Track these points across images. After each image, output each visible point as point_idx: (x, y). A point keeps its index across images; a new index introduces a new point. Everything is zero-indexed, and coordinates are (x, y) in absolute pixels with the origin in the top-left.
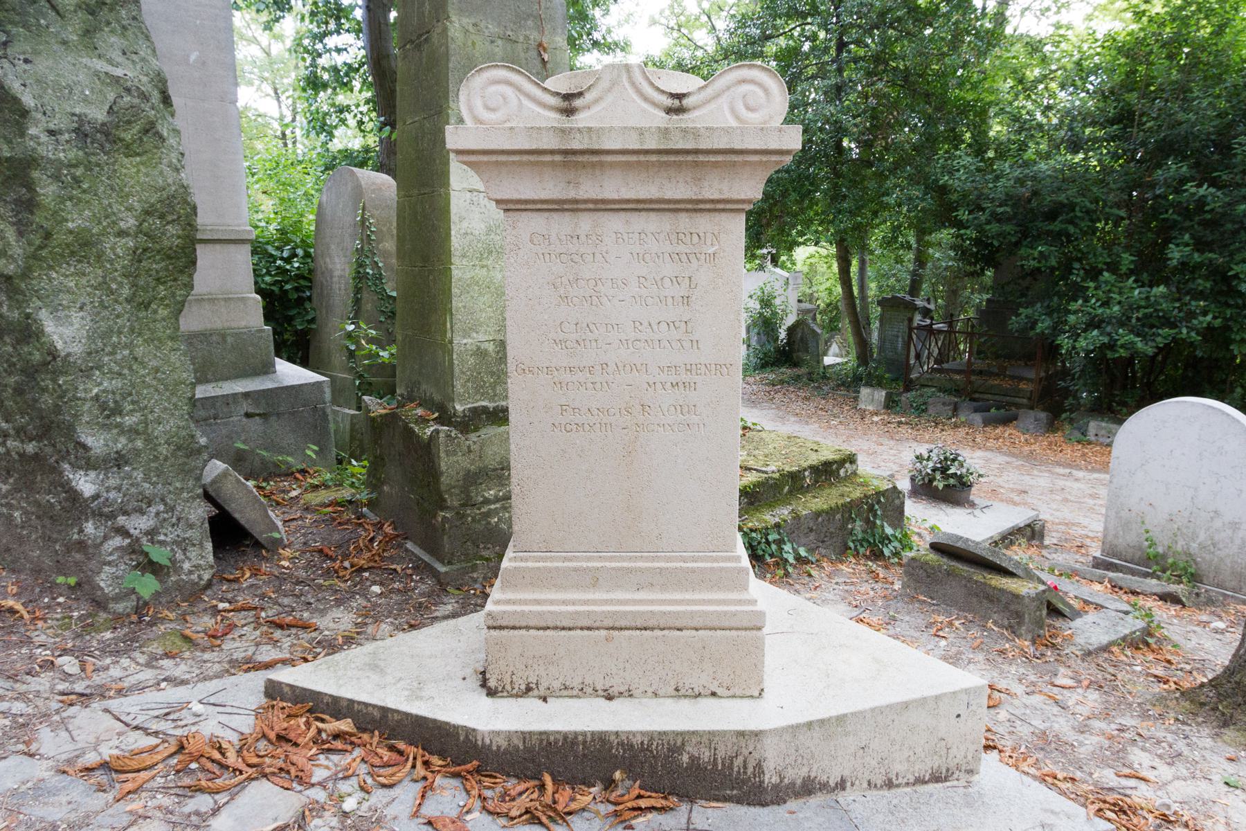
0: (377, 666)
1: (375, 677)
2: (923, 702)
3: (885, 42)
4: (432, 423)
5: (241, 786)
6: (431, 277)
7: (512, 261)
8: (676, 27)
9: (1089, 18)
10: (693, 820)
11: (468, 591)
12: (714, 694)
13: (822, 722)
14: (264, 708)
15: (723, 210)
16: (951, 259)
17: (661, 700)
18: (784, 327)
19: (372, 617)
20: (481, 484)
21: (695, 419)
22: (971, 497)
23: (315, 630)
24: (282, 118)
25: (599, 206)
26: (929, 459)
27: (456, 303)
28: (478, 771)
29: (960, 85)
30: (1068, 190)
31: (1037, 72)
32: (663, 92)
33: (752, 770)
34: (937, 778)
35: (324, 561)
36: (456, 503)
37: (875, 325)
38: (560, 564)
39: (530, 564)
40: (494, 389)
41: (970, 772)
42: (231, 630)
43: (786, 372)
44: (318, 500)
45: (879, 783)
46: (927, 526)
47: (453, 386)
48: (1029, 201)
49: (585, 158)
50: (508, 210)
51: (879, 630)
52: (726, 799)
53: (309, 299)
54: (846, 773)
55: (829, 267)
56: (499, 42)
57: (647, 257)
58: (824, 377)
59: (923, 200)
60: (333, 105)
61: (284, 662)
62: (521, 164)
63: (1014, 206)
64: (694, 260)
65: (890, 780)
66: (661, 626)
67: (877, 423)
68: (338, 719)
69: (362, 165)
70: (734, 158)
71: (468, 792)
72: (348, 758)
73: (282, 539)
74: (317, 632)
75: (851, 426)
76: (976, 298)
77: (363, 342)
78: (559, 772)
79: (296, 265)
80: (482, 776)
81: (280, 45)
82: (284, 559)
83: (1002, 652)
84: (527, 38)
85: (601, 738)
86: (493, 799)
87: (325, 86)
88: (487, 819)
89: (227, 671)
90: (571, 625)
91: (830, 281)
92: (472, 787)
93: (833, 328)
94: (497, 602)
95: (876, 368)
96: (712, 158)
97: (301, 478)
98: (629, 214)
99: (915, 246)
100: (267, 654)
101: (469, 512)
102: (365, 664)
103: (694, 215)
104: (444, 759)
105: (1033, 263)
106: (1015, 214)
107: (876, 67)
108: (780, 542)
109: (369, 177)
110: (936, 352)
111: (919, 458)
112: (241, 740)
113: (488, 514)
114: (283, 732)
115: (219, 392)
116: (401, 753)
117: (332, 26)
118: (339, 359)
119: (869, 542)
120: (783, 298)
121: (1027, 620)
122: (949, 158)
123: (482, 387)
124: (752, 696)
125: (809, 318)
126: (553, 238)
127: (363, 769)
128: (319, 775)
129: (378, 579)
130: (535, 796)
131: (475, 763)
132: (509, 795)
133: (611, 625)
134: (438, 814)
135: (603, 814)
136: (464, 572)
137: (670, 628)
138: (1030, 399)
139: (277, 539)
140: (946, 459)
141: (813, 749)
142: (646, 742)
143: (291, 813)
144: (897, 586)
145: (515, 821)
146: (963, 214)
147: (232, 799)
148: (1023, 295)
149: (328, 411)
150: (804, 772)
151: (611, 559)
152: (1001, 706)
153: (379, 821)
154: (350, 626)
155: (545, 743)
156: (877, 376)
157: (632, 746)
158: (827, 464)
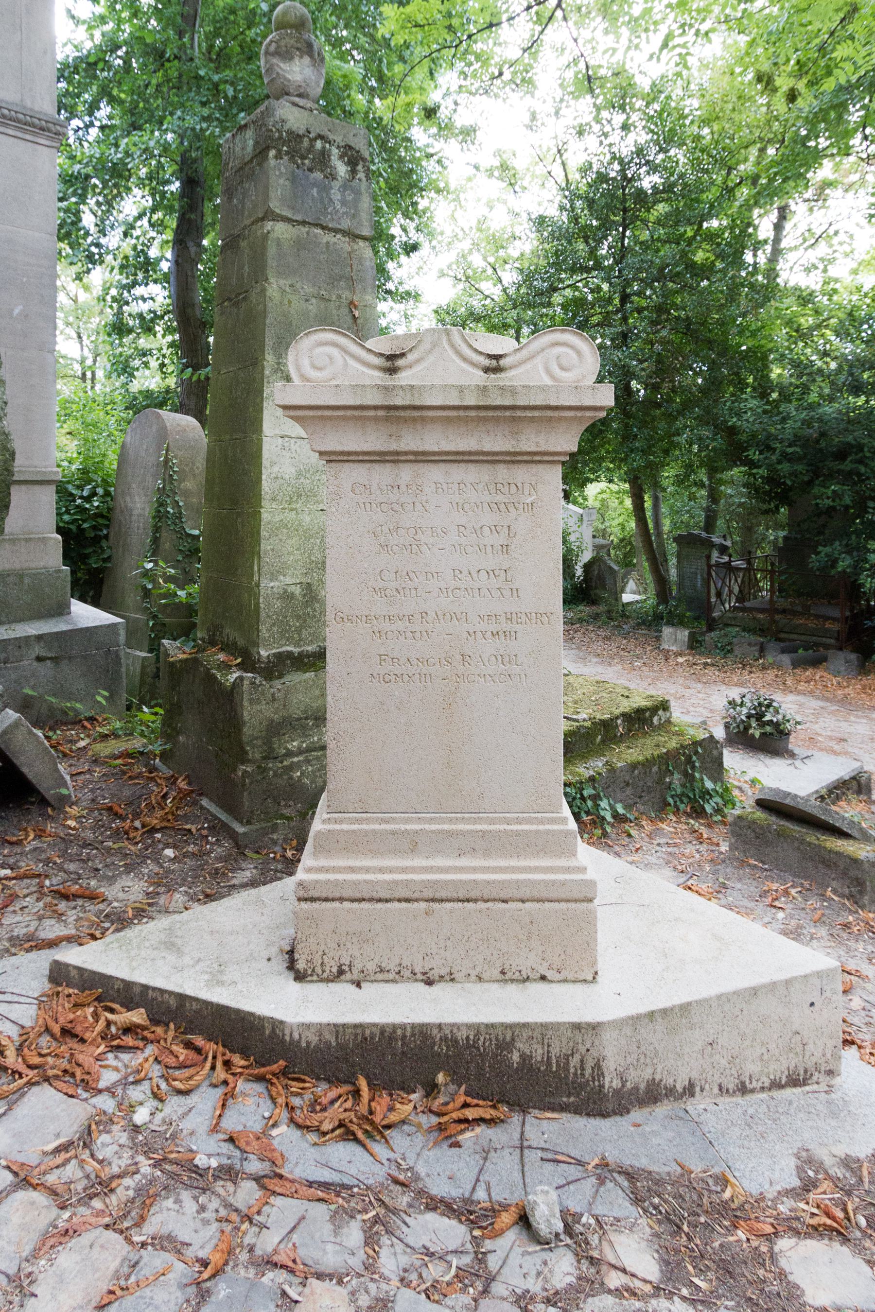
0: (173, 944)
1: (171, 958)
2: (772, 986)
3: (666, 294)
4: (234, 669)
5: (20, 1093)
6: (239, 520)
7: (334, 510)
8: (463, 279)
9: (855, 272)
10: (527, 1135)
11: (267, 854)
12: (543, 978)
13: (665, 1012)
14: (48, 996)
15: (540, 462)
16: (742, 495)
17: (486, 985)
18: (580, 564)
19: (165, 886)
20: (284, 734)
21: (516, 669)
22: (790, 746)
23: (103, 901)
24: (82, 361)
25: (419, 458)
26: (742, 705)
27: (265, 546)
28: (284, 1073)
29: (741, 333)
30: (854, 431)
31: (811, 320)
32: (481, 353)
33: (590, 1071)
34: (795, 1081)
35: (113, 821)
36: (258, 756)
37: (673, 561)
38: (377, 827)
39: (345, 827)
40: (299, 634)
41: (830, 1073)
42: (12, 901)
43: (585, 610)
44: (107, 752)
45: (731, 1087)
46: (747, 778)
47: (258, 630)
48: (817, 441)
49: (408, 413)
50: (331, 461)
51: (709, 900)
52: (563, 1108)
53: (106, 537)
54: (694, 1075)
55: (621, 503)
56: (314, 301)
57: (466, 506)
58: (624, 615)
59: (713, 440)
60: (136, 348)
61: (69, 939)
62: (344, 418)
63: (803, 447)
64: (512, 509)
65: (743, 1084)
66: (485, 898)
67: (682, 664)
68: (129, 1010)
69: (161, 405)
70: (549, 413)
71: (273, 1100)
72: (140, 1057)
73: (69, 796)
74: (105, 904)
75: (656, 668)
76: (771, 535)
77: (161, 581)
78: (375, 1074)
79: (96, 504)
80: (289, 1079)
81: (88, 295)
82: (70, 818)
83: (846, 926)
84: (339, 297)
85: (422, 1031)
86: (302, 1108)
87: (130, 331)
88: (297, 1133)
89: (7, 950)
90: (388, 896)
91: (623, 517)
92: (278, 1093)
93: (627, 564)
94: (309, 870)
95: (676, 606)
96: (529, 414)
97: (89, 726)
98: (448, 465)
99: (707, 483)
100: (51, 929)
101: (270, 765)
102: (160, 943)
103: (511, 466)
104: (246, 1057)
105: (829, 502)
106: (805, 455)
107: (659, 316)
108: (596, 798)
109: (174, 419)
110: (736, 589)
111: (732, 703)
112: (21, 1035)
113: (291, 768)
114: (69, 1025)
115: (12, 635)
116: (198, 1050)
117: (140, 276)
118: (133, 598)
119: (689, 798)
120: (578, 535)
121: (869, 889)
122: (736, 401)
123: (287, 631)
124: (585, 981)
125: (603, 553)
126: (374, 487)
127: (156, 1071)
128: (108, 1078)
129: (171, 841)
130: (349, 1104)
131: (282, 1063)
132: (320, 1104)
133: (431, 896)
134: (241, 1128)
135: (425, 1127)
136: (265, 832)
137: (494, 900)
138: (837, 639)
139: (64, 796)
140: (760, 704)
141: (657, 1045)
142: (471, 1037)
143: (75, 1128)
144: (724, 847)
145: (327, 1137)
146: (754, 455)
147: (10, 1109)
148: (820, 533)
149: (122, 654)
150: (647, 1074)
151: (431, 821)
152: (853, 991)
153: (174, 1136)
154: (141, 896)
155: (360, 1038)
156: (678, 615)
157: (456, 1041)
158: (640, 711)
